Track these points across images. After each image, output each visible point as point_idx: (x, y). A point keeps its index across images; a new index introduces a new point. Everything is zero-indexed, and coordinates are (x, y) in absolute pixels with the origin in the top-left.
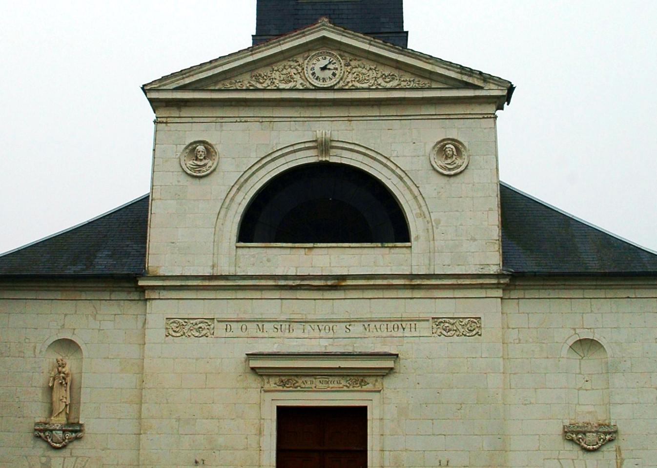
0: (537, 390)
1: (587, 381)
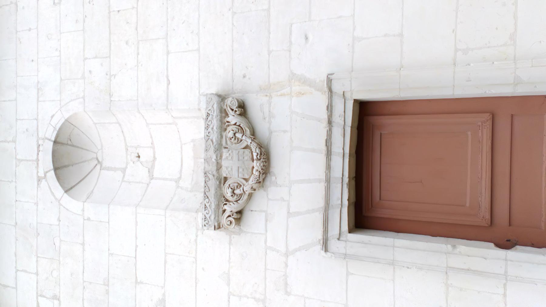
0: (139, 281)
1: (139, 157)
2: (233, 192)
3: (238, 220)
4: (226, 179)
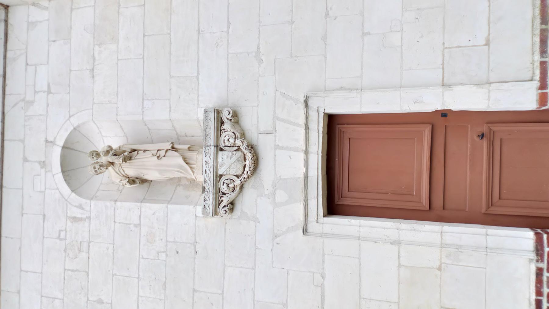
2: (228, 186)
3: (232, 210)
4: (221, 176)
